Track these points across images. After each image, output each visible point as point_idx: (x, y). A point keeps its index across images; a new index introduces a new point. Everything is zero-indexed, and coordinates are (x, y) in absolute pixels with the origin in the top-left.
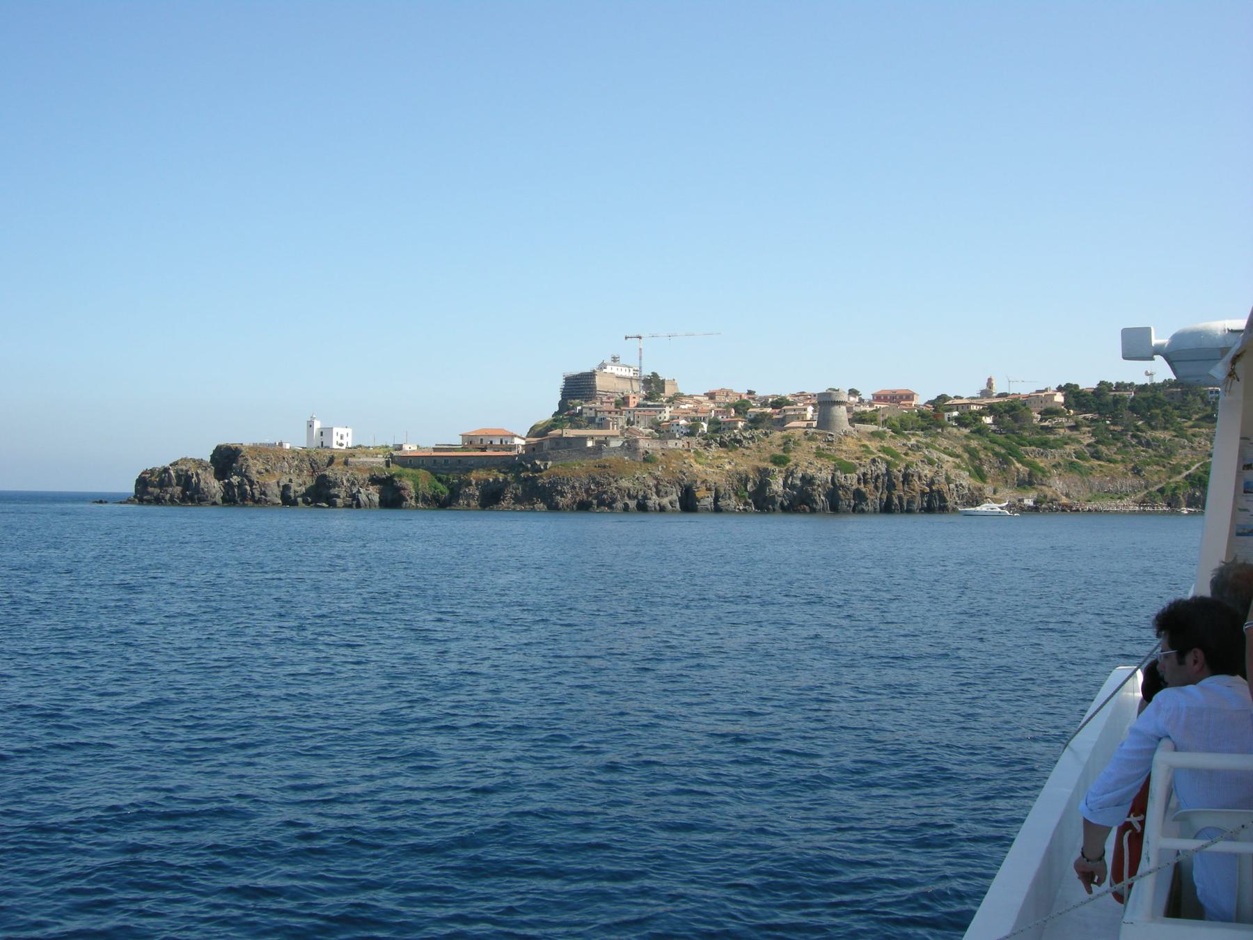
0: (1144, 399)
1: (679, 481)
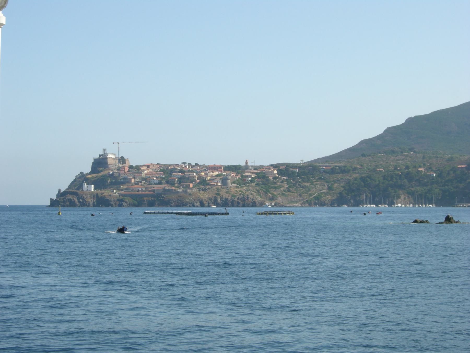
0: (301, 172)
1: (199, 200)
